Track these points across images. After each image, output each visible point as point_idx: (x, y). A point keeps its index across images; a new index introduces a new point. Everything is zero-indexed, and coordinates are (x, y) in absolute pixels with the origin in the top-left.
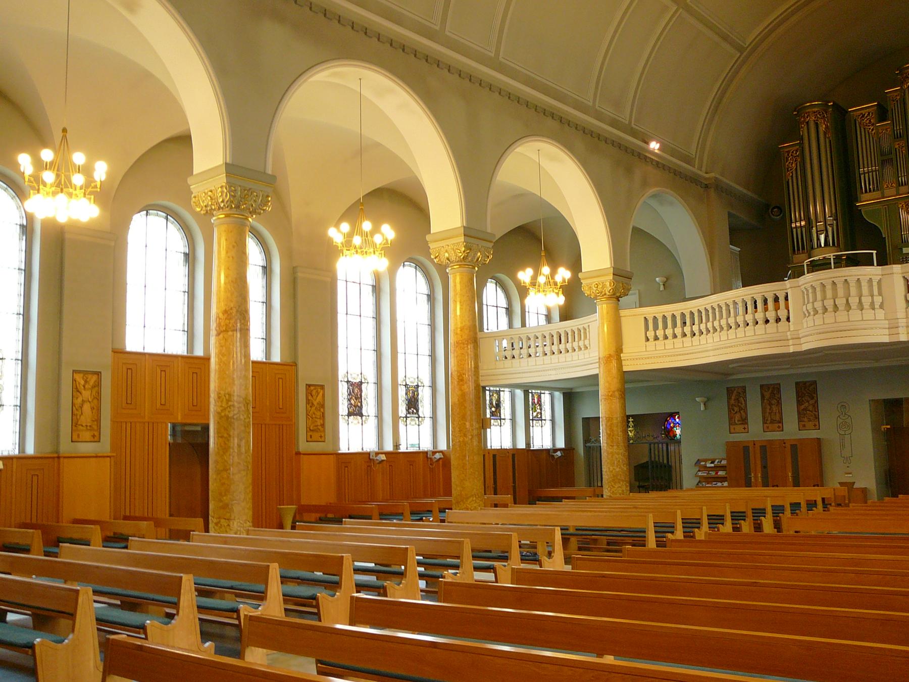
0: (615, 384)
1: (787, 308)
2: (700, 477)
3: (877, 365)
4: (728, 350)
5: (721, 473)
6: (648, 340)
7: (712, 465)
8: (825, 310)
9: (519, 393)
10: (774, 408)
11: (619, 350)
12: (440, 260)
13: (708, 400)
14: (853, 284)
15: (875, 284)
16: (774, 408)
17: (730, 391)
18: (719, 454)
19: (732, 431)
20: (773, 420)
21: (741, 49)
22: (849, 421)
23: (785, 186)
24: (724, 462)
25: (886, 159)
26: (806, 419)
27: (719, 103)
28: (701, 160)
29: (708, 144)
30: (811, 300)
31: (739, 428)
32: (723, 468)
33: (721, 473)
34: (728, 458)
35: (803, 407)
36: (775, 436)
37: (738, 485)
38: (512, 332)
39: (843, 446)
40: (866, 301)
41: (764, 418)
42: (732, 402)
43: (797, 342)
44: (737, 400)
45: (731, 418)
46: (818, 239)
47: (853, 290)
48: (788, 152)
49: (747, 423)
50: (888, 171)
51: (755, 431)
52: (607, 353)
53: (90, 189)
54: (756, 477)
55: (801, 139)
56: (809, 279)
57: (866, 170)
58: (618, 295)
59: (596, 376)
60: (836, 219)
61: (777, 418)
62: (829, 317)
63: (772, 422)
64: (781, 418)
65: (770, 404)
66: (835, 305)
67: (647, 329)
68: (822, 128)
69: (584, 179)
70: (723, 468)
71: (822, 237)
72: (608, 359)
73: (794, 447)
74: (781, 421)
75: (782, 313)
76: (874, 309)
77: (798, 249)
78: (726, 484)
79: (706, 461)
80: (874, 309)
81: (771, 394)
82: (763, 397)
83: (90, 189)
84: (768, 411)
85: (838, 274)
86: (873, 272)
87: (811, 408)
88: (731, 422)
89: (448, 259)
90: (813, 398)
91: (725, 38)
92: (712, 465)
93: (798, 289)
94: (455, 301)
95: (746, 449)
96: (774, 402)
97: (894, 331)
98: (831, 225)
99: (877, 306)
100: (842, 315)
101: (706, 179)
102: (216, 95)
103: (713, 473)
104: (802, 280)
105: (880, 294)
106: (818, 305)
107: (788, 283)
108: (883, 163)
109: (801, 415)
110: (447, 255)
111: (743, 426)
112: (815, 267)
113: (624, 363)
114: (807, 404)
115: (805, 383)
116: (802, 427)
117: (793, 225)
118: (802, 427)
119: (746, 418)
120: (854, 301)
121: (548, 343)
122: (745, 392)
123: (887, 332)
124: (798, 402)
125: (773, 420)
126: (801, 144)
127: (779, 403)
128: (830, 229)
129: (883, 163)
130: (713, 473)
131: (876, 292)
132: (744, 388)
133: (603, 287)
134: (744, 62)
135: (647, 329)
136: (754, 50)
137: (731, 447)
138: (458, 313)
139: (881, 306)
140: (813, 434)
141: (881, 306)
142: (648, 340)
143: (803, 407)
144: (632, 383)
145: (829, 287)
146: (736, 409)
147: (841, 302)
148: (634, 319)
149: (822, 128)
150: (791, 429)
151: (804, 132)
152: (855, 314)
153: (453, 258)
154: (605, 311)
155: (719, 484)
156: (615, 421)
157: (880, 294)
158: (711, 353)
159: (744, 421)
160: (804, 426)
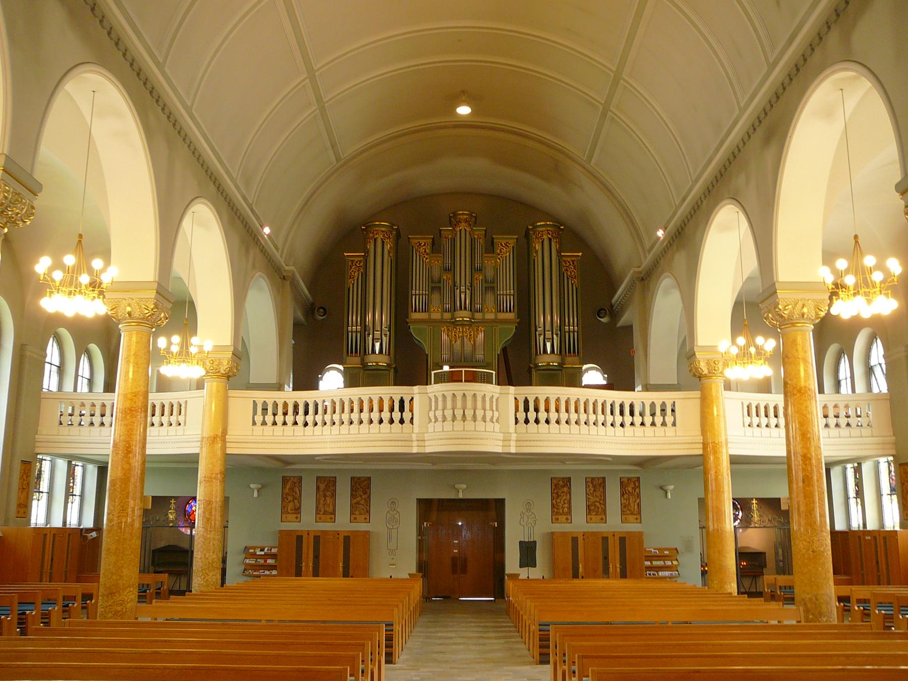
0: (218, 467)
1: (411, 410)
2: (246, 564)
3: (434, 467)
4: (350, 444)
5: (270, 561)
6: (254, 423)
7: (263, 553)
8: (444, 419)
9: (62, 465)
10: (328, 500)
11: (225, 432)
12: (117, 312)
13: (263, 486)
14: (469, 399)
15: (487, 399)
16: (328, 500)
17: (285, 480)
18: (270, 543)
19: (284, 518)
20: (326, 510)
21: (338, 159)
22: (397, 516)
23: (346, 292)
24: (274, 551)
25: (435, 286)
26: (357, 513)
27: (308, 201)
28: (283, 249)
29: (290, 238)
30: (433, 408)
31: (291, 517)
32: (274, 556)
33: (270, 561)
34: (280, 546)
35: (355, 501)
36: (327, 526)
37: (288, 574)
38: (91, 396)
39: (390, 538)
40: (480, 413)
41: (317, 508)
42: (287, 491)
43: (421, 443)
44: (292, 489)
45: (283, 507)
46: (373, 345)
47: (469, 404)
48: (353, 261)
49: (300, 513)
50: (436, 297)
51: (308, 521)
52: (212, 434)
53: (887, 284)
54: (307, 566)
55: (367, 252)
56: (435, 389)
57: (418, 293)
58: (230, 374)
59: (197, 455)
60: (390, 331)
61: (330, 509)
62: (448, 425)
63: (325, 513)
64: (334, 510)
65: (325, 496)
66: (516, 419)
67: (255, 413)
68: (388, 247)
69: (224, 252)
70: (274, 556)
71: (377, 345)
72: (213, 440)
73: (347, 539)
74: (334, 513)
75: (407, 415)
76: (485, 422)
77: (352, 352)
78: (274, 572)
79: (254, 548)
80: (485, 422)
81: (327, 486)
82: (318, 488)
83: (887, 284)
84: (322, 502)
85: (467, 388)
86: (491, 390)
87: (363, 502)
88: (284, 510)
89: (129, 314)
90: (366, 493)
91: (333, 146)
92: (263, 553)
93: (420, 396)
94: (128, 362)
95: (300, 538)
96: (328, 494)
97: (506, 443)
98: (386, 335)
99: (488, 419)
100: (459, 424)
101: (285, 271)
102: (780, 185)
103: (262, 561)
104: (430, 388)
105: (497, 410)
106: (439, 413)
107: (416, 389)
108: (433, 289)
109: (353, 508)
110: (129, 309)
111: (295, 516)
112: (440, 379)
113: (228, 445)
114: (359, 499)
115: (359, 478)
116: (353, 520)
117: (350, 328)
118: (353, 520)
119: (300, 508)
120: (469, 413)
121: (98, 413)
122: (335, 484)
123: (501, 443)
124: (352, 495)
125: (326, 510)
126: (366, 258)
127: (334, 495)
128: (384, 338)
129: (433, 289)
130: (262, 561)
131: (488, 407)
132: (300, 479)
133: (218, 365)
134: (338, 169)
135: (255, 413)
136: (345, 163)
137: (284, 535)
138: (131, 375)
139: (497, 421)
140: (363, 527)
141: (497, 421)
142: (254, 423)
143: (355, 501)
144: (241, 470)
145: (449, 399)
146: (290, 498)
147: (458, 413)
148: (242, 403)
149: (388, 247)
150: (343, 521)
151: (371, 246)
152: (469, 424)
153: (137, 314)
154: (214, 389)
155: (267, 572)
156: (214, 505)
157: (497, 410)
158: (328, 445)
159: (297, 510)
160: (355, 519)
